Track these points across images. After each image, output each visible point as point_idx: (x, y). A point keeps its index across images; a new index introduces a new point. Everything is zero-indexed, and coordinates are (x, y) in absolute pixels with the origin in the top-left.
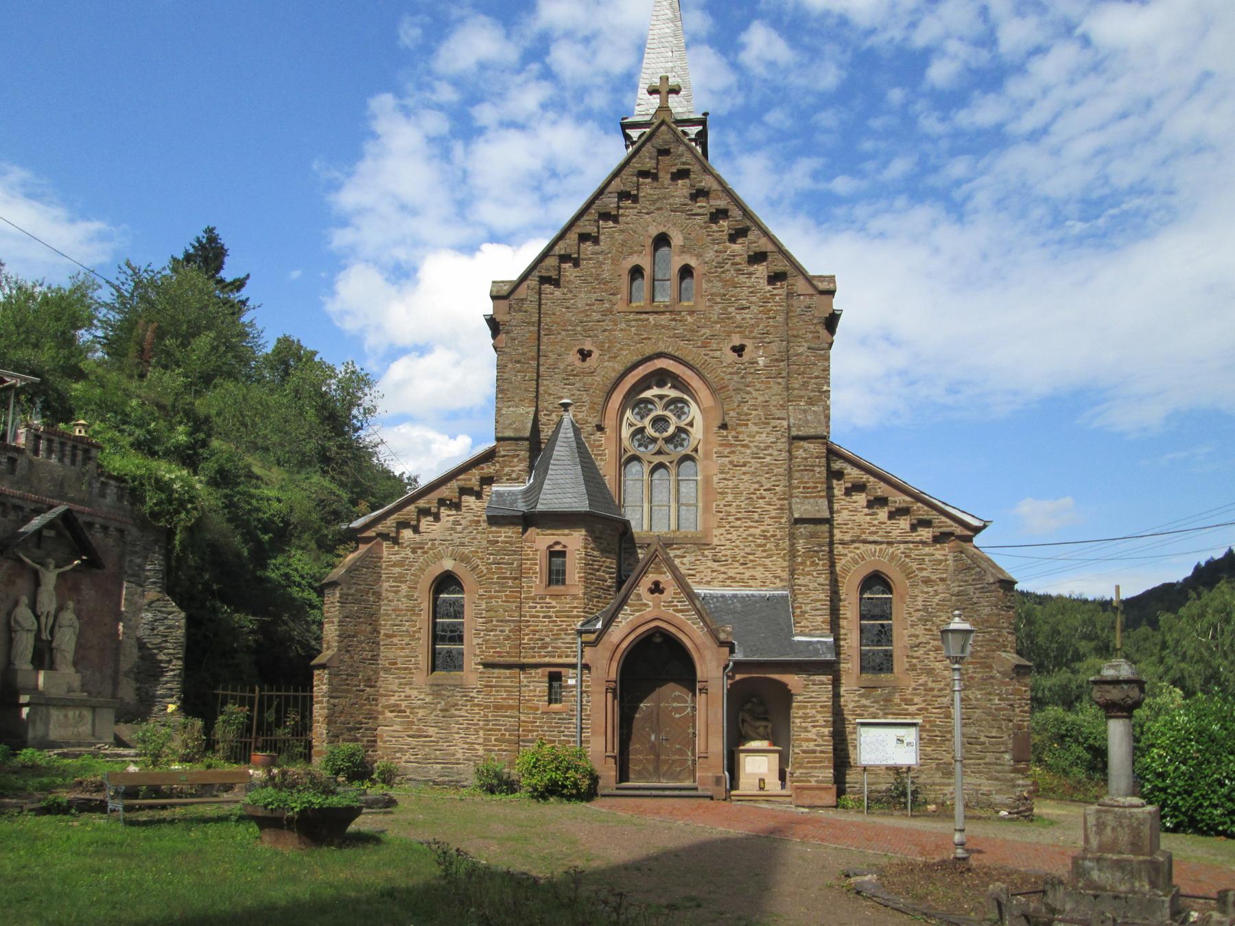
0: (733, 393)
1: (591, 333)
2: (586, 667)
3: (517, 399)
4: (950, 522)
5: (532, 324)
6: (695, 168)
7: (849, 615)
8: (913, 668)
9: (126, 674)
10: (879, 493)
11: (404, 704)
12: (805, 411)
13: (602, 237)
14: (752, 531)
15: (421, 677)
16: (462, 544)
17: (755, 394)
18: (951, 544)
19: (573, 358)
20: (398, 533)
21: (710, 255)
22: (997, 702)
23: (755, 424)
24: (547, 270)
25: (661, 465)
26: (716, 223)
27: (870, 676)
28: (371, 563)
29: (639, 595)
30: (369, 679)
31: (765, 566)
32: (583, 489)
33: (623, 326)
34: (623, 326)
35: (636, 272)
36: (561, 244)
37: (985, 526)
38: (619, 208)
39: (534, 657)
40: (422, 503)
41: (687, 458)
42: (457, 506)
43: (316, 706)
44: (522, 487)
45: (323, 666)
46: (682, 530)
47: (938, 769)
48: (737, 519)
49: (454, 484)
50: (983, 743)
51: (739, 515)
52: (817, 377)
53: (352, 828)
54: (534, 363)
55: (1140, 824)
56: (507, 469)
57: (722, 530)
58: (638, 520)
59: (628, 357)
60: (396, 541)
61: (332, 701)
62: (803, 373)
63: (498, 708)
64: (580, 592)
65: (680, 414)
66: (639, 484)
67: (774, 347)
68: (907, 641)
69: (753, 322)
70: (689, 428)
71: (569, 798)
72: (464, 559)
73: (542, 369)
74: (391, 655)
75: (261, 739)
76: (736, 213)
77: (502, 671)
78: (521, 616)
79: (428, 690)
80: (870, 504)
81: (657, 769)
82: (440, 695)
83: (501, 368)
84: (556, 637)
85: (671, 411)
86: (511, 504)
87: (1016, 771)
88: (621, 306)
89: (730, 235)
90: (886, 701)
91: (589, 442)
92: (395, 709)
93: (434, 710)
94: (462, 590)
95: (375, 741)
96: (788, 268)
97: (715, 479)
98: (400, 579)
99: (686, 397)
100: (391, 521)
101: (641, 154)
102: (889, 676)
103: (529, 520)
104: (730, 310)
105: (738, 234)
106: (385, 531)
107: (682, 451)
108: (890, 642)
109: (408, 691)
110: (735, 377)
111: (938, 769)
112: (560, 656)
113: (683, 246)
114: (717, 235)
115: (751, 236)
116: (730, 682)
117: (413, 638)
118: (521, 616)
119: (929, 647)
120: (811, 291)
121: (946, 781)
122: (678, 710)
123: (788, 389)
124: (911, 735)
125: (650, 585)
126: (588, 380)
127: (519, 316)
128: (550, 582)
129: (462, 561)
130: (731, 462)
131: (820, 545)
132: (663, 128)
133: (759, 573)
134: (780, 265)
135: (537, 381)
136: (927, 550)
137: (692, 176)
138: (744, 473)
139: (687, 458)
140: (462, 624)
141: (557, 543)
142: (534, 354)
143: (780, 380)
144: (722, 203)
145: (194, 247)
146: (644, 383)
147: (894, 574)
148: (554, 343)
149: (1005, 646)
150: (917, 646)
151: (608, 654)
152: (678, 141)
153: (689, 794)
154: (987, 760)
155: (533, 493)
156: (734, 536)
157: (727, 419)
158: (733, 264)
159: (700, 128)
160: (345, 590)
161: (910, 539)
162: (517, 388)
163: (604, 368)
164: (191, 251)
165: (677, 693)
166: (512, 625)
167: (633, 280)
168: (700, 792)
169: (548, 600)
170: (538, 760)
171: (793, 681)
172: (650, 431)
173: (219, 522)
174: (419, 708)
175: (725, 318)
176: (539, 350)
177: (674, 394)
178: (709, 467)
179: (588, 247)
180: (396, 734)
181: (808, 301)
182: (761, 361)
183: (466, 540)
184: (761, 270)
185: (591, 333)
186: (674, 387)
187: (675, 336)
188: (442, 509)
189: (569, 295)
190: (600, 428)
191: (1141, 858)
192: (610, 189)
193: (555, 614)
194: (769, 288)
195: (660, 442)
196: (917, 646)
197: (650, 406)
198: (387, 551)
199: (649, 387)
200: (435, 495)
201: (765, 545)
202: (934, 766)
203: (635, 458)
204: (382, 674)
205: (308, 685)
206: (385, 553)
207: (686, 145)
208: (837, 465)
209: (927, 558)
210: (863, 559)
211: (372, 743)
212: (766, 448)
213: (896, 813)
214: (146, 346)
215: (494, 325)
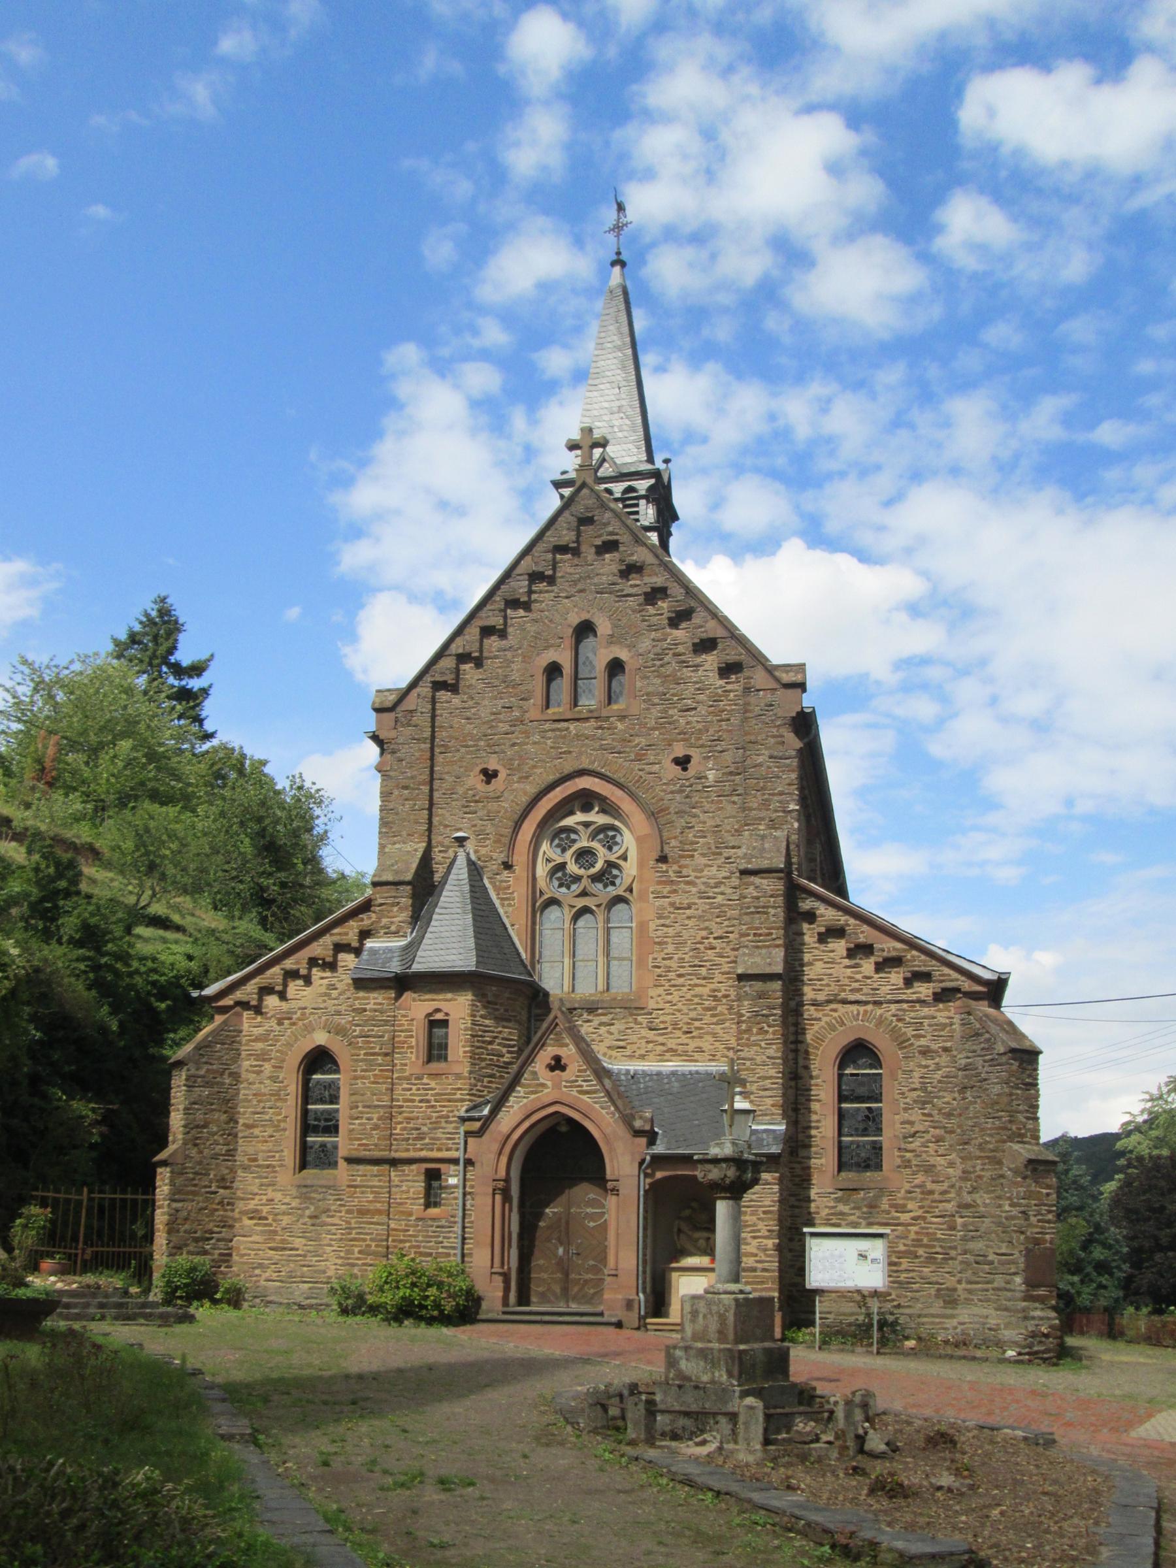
0: (674, 817)
1: (497, 749)
2: (469, 1162)
3: (404, 833)
4: (955, 975)
5: (424, 740)
6: (624, 538)
7: (823, 1096)
8: (907, 1164)
10: (862, 939)
11: (265, 1209)
12: (763, 837)
13: (510, 630)
14: (698, 990)
15: (286, 1176)
16: (338, 1013)
17: (702, 817)
18: (958, 1003)
19: (474, 780)
20: (260, 1000)
21: (645, 644)
22: (1007, 1208)
23: (703, 855)
24: (442, 673)
25: (585, 910)
26: (653, 604)
27: (851, 1175)
28: (229, 1038)
29: (535, 1073)
30: (223, 1179)
31: (714, 1035)
32: (471, 943)
33: (537, 738)
34: (537, 738)
35: (553, 670)
36: (459, 641)
38: (530, 592)
39: (408, 1150)
40: (289, 964)
41: (619, 899)
42: (332, 966)
43: (158, 1212)
44: (403, 942)
45: (164, 1163)
46: (613, 991)
47: (937, 1296)
48: (680, 976)
50: (992, 1263)
51: (682, 971)
52: (781, 794)
53: (48, 1323)
54: (426, 789)
55: (726, 1311)
56: (384, 921)
57: (660, 990)
58: (553, 979)
60: (258, 1010)
61: (175, 1205)
62: (763, 788)
63: (362, 1212)
64: (465, 1069)
65: (610, 846)
66: (559, 934)
67: (728, 757)
68: (900, 1130)
69: (699, 726)
70: (621, 862)
71: (430, 1321)
72: (340, 1031)
73: (436, 795)
74: (251, 1150)
75: (89, 1251)
76: (676, 591)
77: (369, 1167)
78: (392, 1100)
79: (294, 1192)
80: (851, 953)
81: (565, 1290)
82: (310, 1198)
83: (385, 795)
84: (436, 1126)
85: (600, 841)
87: (1028, 1298)
88: (534, 713)
89: (670, 619)
90: (871, 1206)
92: (256, 1215)
93: (302, 1216)
94: (337, 1071)
95: (230, 1255)
96: (743, 657)
97: (652, 926)
98: (263, 1057)
99: (617, 823)
100: (252, 987)
101: (556, 525)
102: (876, 1174)
103: (403, 983)
104: (671, 712)
105: (679, 618)
106: (245, 998)
107: (612, 891)
108: (879, 1131)
110: (678, 797)
111: (937, 1296)
112: (439, 1150)
113: (612, 636)
114: (654, 620)
115: (697, 619)
116: (648, 1181)
117: (277, 1128)
118: (392, 1100)
119: (927, 1137)
121: (949, 1312)
122: (592, 1217)
123: (744, 809)
124: (877, 1249)
125: (548, 1061)
126: (493, 806)
128: (430, 1059)
129: (337, 1034)
130: (672, 904)
131: (770, 1008)
132: (585, 491)
133: (706, 1043)
134: (734, 654)
135: (430, 809)
136: (926, 1011)
137: (622, 548)
138: (689, 918)
139: (619, 899)
140: (337, 1111)
141: (438, 1010)
142: (425, 777)
143: (735, 798)
144: (659, 580)
145: (141, 623)
146: (565, 807)
147: (881, 1042)
148: (453, 763)
149: (1022, 1136)
150: (913, 1136)
151: (495, 1147)
152: (603, 506)
153: (595, 1320)
154: (996, 1285)
155: (411, 950)
156: (675, 997)
157: (667, 849)
158: (675, 655)
159: (652, 481)
160: (193, 1071)
161: (904, 997)
162: (404, 820)
163: (513, 791)
165: (591, 1196)
166: (382, 1111)
167: (549, 681)
168: (605, 1319)
169: (425, 1081)
170: (390, 1274)
171: (443, 1167)
172: (573, 868)
173: (76, 990)
174: (284, 1214)
175: (665, 723)
176: (432, 772)
177: (601, 819)
178: (644, 909)
179: (493, 643)
180: (256, 1246)
181: (769, 697)
182: (711, 775)
183: (343, 1008)
184: (710, 660)
185: (497, 749)
186: (603, 811)
187: (602, 748)
188: (314, 970)
189: (471, 703)
190: (507, 866)
192: (518, 570)
193: (424, 1094)
194: (722, 682)
195: (585, 882)
196: (913, 1136)
197: (573, 836)
198: (248, 1023)
199: (572, 813)
201: (715, 1008)
202: (933, 1292)
203: (553, 902)
204: (240, 1173)
205: (149, 1186)
206: (245, 1026)
207: (612, 510)
208: (806, 905)
210: (842, 1024)
211: (226, 1258)
212: (717, 885)
213: (859, 1349)
214: (48, 764)
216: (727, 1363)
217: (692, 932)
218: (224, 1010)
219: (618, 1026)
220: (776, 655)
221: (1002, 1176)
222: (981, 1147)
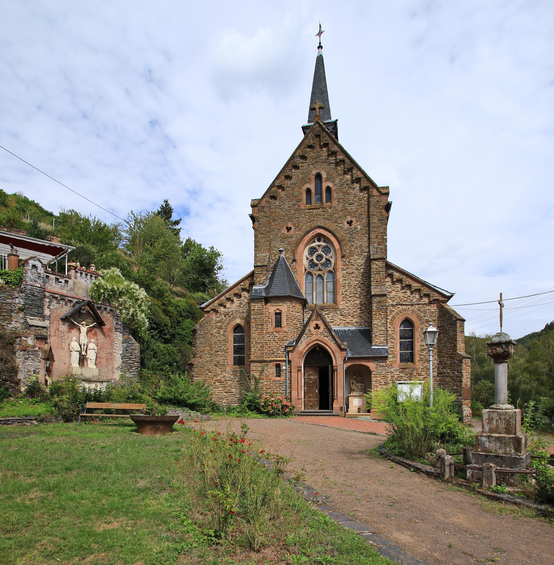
4: (437, 295)
9: (117, 369)
12: (377, 248)
17: (356, 242)
19: (284, 231)
23: (357, 255)
27: (404, 364)
29: (310, 330)
37: (452, 296)
40: (227, 295)
48: (350, 297)
49: (239, 287)
51: (351, 295)
52: (382, 233)
59: (305, 228)
74: (217, 359)
79: (231, 373)
83: (256, 236)
86: (260, 293)
90: (410, 374)
91: (291, 267)
98: (220, 328)
109: (224, 374)
110: (348, 235)
112: (280, 357)
120: (378, 194)
126: (290, 240)
127: (262, 214)
144: (340, 157)
147: (414, 319)
148: (276, 225)
164: (160, 210)
171: (371, 365)
175: (344, 209)
181: (378, 199)
182: (359, 227)
186: (324, 241)
189: (282, 204)
191: (510, 436)
194: (362, 194)
195: (320, 265)
199: (314, 242)
200: (232, 292)
209: (428, 311)
215: (252, 217)
216: (514, 444)
217: (354, 282)
218: (208, 312)
219: (332, 314)
220: (380, 184)
221: (454, 363)
222: (446, 353)
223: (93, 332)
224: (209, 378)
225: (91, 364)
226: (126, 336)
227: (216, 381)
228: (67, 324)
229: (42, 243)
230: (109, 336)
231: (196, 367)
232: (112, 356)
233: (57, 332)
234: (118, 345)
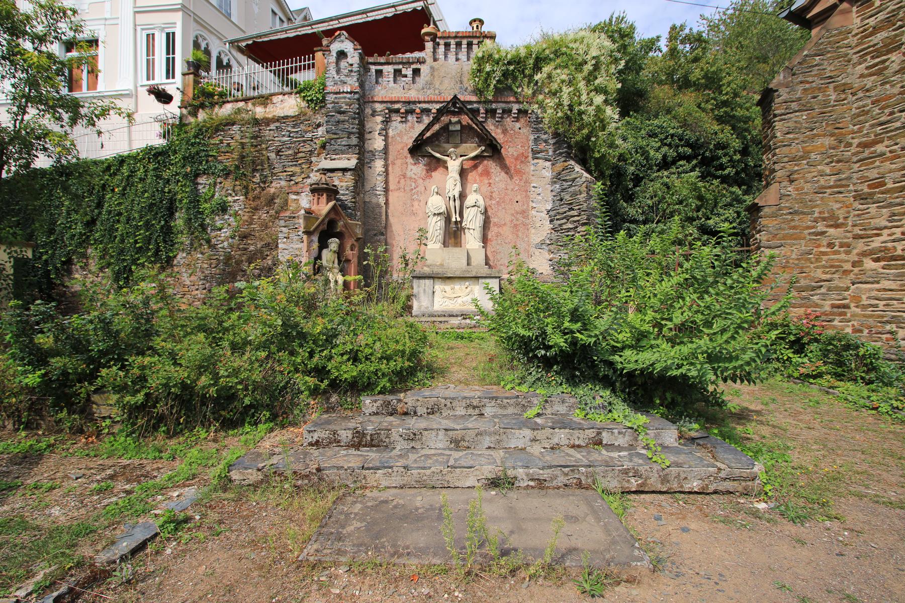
74: (873, 174)
223: (480, 169)
224: (831, 245)
225: (472, 240)
226: (559, 166)
227: (864, 254)
228: (423, 161)
229: (382, 16)
230: (518, 172)
231: (774, 216)
232: (527, 217)
233: (402, 181)
234: (539, 190)
